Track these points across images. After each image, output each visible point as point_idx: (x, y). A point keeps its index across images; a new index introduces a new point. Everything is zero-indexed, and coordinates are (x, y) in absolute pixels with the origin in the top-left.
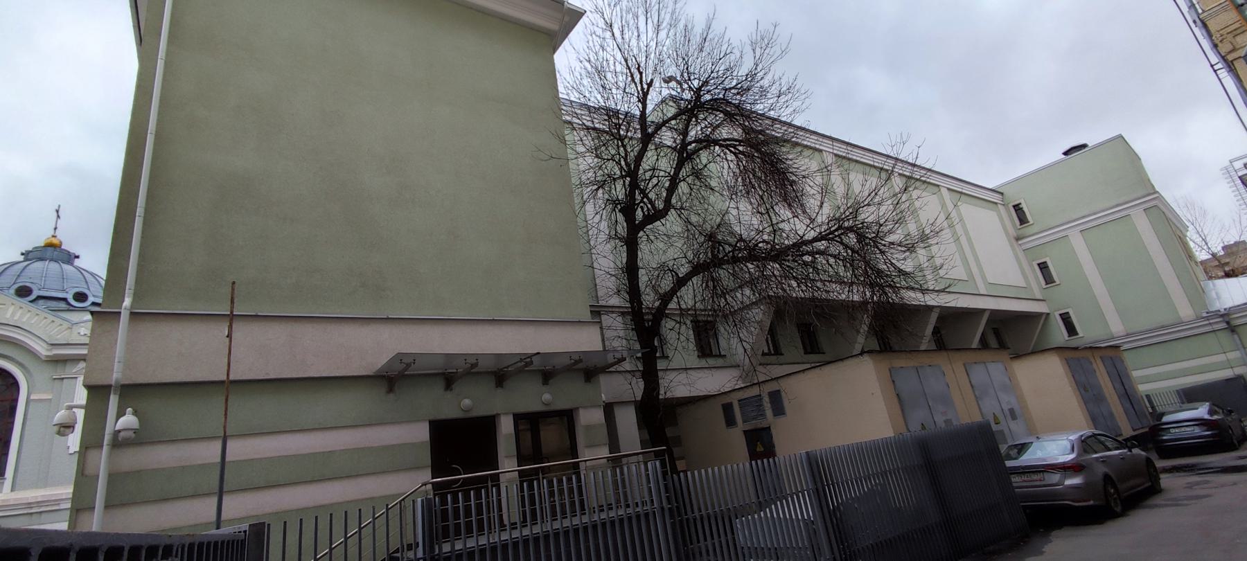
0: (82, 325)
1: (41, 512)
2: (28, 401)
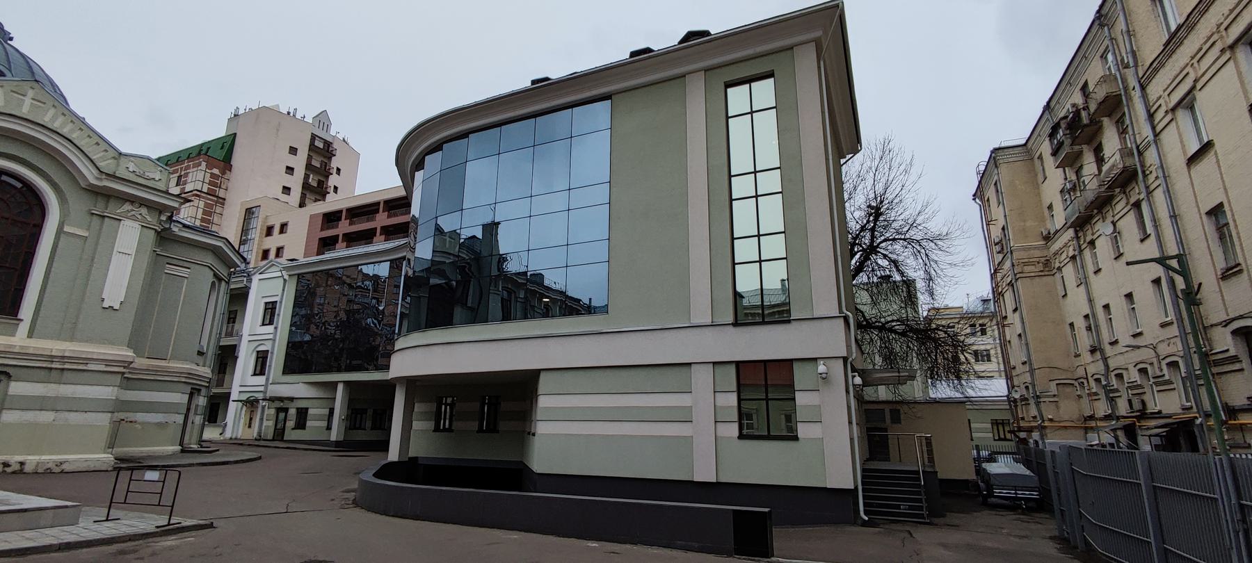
0: (132, 159)
1: (63, 369)
2: (60, 231)
